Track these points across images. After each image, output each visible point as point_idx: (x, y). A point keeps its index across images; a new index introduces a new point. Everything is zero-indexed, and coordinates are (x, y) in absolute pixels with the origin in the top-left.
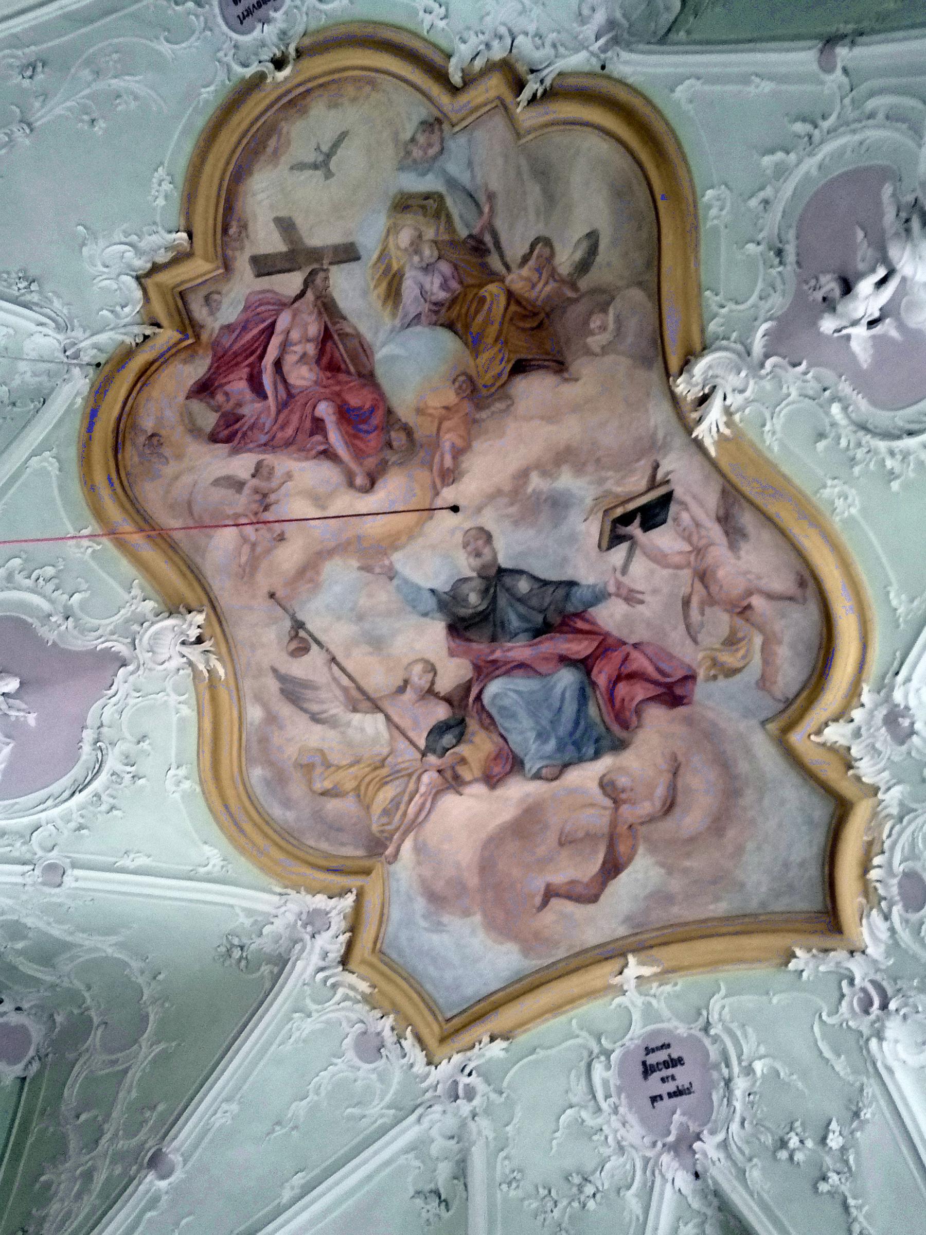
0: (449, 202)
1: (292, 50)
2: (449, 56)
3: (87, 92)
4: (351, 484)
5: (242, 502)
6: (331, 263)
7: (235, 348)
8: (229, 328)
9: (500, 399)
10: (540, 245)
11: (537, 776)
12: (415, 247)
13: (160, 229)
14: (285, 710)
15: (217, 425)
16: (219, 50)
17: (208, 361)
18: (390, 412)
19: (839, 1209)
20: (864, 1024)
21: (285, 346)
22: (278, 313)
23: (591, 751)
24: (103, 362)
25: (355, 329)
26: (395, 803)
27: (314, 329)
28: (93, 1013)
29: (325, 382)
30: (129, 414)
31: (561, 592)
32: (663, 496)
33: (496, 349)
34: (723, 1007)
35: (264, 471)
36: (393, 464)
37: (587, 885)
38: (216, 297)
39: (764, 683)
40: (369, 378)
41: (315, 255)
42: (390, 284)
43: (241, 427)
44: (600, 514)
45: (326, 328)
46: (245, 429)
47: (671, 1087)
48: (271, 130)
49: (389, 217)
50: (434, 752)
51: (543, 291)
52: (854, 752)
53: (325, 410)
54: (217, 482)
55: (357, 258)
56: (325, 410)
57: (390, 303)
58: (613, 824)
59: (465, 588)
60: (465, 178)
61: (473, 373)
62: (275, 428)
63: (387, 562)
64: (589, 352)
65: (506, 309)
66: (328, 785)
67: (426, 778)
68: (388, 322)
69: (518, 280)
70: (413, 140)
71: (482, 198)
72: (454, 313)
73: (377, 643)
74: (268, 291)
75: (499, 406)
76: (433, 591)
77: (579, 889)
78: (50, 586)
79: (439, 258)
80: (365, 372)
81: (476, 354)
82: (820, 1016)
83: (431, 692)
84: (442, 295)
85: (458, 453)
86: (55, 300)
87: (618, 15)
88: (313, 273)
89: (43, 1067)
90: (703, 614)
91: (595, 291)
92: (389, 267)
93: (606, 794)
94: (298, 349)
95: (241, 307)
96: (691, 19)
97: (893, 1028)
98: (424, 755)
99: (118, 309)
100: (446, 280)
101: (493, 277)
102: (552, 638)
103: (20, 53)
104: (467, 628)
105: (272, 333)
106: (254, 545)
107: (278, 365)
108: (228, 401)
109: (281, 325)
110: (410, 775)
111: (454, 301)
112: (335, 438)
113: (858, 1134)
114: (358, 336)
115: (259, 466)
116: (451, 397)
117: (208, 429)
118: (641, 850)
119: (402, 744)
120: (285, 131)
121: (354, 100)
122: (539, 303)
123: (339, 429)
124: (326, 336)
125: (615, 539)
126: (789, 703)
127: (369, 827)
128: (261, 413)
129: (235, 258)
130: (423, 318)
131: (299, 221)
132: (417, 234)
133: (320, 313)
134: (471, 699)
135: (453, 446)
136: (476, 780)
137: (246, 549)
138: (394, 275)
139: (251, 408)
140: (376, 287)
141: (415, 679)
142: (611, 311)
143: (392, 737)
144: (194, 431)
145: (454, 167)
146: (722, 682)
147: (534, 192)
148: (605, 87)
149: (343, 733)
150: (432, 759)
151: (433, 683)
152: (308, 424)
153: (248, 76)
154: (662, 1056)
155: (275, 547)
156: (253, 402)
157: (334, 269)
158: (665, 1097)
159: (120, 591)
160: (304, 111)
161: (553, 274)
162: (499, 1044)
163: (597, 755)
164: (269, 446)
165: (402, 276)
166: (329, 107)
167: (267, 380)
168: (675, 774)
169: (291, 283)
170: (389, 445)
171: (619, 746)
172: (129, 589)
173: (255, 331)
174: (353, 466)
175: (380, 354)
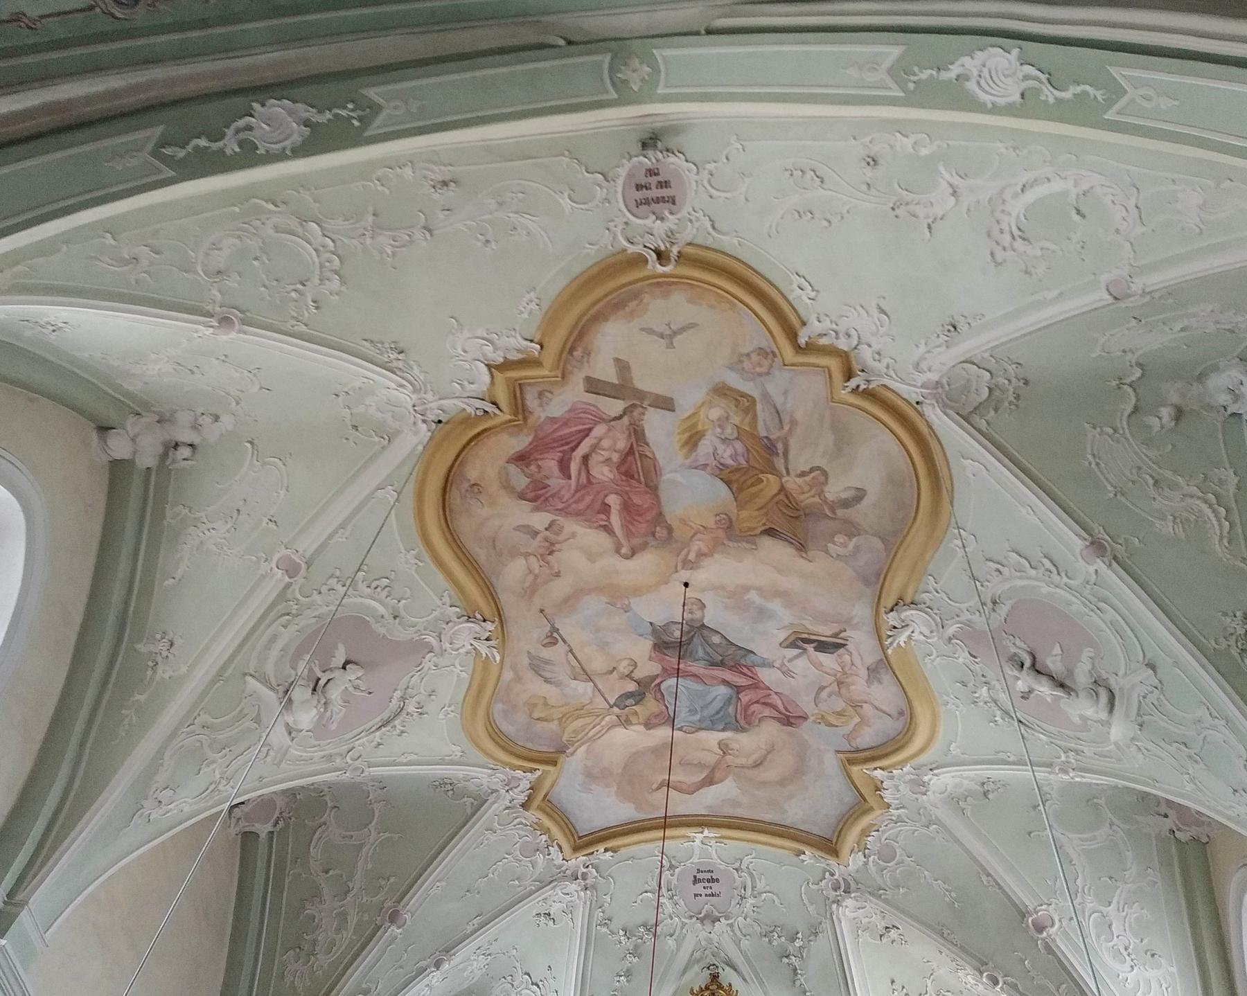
0: (759, 407)
1: (675, 250)
2: (804, 324)
3: (488, 217)
4: (618, 551)
5: (535, 544)
6: (649, 405)
7: (555, 435)
8: (553, 420)
9: (747, 542)
10: (819, 472)
12: (722, 422)
13: (518, 335)
14: (529, 675)
15: (527, 487)
16: (612, 221)
17: (530, 439)
18: (660, 514)
19: (791, 972)
21: (594, 448)
22: (596, 423)
23: (721, 727)
24: (443, 421)
25: (654, 454)
26: (583, 728)
27: (622, 444)
28: (327, 798)
29: (620, 483)
30: (459, 465)
31: (742, 652)
32: (841, 644)
33: (756, 513)
34: (751, 863)
35: (555, 528)
36: (652, 546)
37: (689, 785)
38: (547, 394)
39: (849, 737)
40: (653, 489)
41: (640, 395)
42: (690, 437)
43: (547, 492)
44: (791, 631)
45: (632, 445)
46: (547, 495)
47: (709, 891)
48: (636, 295)
49: (708, 394)
50: (618, 706)
51: (808, 499)
52: (884, 785)
53: (613, 500)
54: (517, 528)
55: (673, 410)
56: (613, 500)
57: (685, 450)
58: (718, 763)
59: (674, 627)
60: (779, 400)
61: (734, 519)
62: (571, 501)
63: (627, 602)
64: (827, 552)
65: (776, 495)
66: (542, 715)
67: (607, 719)
68: (680, 459)
69: (791, 483)
70: (748, 355)
71: (786, 419)
72: (735, 477)
73: (603, 646)
74: (594, 406)
75: (748, 546)
76: (651, 623)
77: (684, 787)
78: (385, 593)
79: (737, 439)
80: (651, 484)
81: (741, 505)
82: (808, 883)
83: (629, 676)
84: (729, 462)
85: (701, 555)
86: (415, 368)
87: (944, 381)
88: (634, 406)
89: (287, 826)
90: (829, 696)
91: (846, 521)
92: (695, 425)
93: (720, 748)
94: (606, 454)
95: (566, 408)
96: (992, 413)
97: (849, 902)
98: (611, 707)
99: (466, 383)
100: (736, 454)
101: (774, 471)
102: (723, 670)
103: (436, 169)
104: (666, 648)
105: (587, 435)
106: (536, 577)
107: (586, 459)
108: (539, 472)
109: (599, 430)
110: (598, 716)
111: (737, 470)
112: (615, 520)
113: (812, 943)
114: (654, 459)
116: (711, 523)
117: (519, 489)
118: (730, 778)
119: (599, 700)
120: (645, 301)
121: (712, 307)
122: (803, 504)
123: (620, 516)
124: (631, 451)
125: (793, 645)
126: (858, 751)
127: (561, 738)
128: (563, 487)
129: (572, 373)
130: (709, 468)
131: (633, 367)
132: (726, 415)
133: (630, 435)
134: (653, 685)
135: (699, 550)
136: (639, 724)
137: (531, 578)
138: (697, 432)
139: (556, 482)
140: (679, 434)
141: (621, 668)
142: (854, 540)
143: (594, 695)
144: (507, 486)
145: (771, 388)
146: (823, 727)
147: (828, 439)
149: (562, 690)
150: (616, 710)
151: (632, 672)
152: (597, 506)
153: (629, 251)
154: (708, 876)
155: (551, 580)
156: (558, 478)
157: (651, 410)
158: (703, 895)
159: (435, 598)
160: (666, 295)
161: (820, 494)
162: (609, 854)
163: (723, 730)
164: (565, 512)
165: (704, 435)
166: (689, 301)
167: (574, 467)
168: (769, 753)
169: (615, 407)
170: (654, 535)
171: (740, 729)
172: (441, 598)
173: (574, 429)
174: (623, 541)
175: (666, 477)
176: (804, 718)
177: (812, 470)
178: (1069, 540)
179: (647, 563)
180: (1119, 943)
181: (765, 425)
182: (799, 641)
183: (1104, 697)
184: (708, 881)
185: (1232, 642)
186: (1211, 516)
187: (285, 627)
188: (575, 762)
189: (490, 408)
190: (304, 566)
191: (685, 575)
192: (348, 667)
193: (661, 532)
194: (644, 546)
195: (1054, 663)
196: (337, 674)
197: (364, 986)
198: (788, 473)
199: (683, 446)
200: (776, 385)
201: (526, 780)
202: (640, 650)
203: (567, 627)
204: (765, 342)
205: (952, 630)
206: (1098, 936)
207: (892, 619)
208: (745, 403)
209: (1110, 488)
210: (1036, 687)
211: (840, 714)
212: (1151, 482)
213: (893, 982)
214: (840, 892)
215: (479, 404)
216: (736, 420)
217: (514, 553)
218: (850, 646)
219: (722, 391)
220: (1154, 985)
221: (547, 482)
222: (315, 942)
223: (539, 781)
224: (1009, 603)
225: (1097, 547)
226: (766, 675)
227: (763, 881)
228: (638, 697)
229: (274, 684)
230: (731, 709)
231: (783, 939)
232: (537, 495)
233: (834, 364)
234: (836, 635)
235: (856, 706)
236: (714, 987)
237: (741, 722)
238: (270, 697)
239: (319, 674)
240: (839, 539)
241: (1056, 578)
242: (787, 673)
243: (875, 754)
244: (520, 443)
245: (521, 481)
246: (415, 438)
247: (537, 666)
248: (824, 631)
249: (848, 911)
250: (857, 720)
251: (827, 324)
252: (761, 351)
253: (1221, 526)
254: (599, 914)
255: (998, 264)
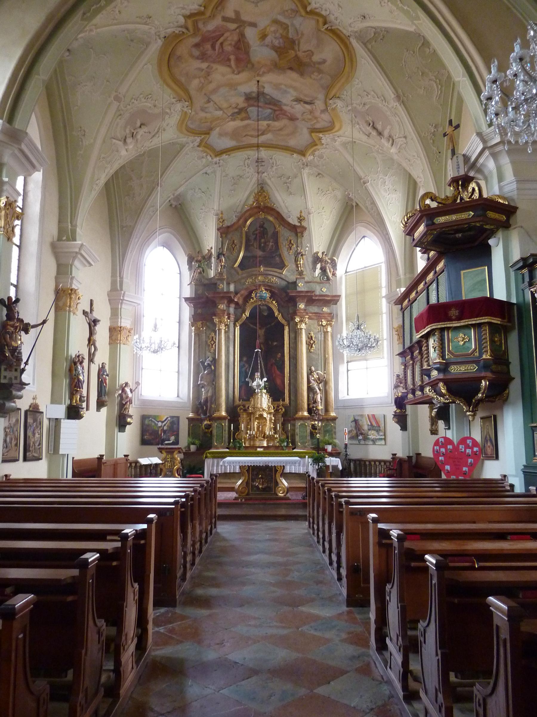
0: (290, 28)
4: (233, 72)
8: (209, 31)
11: (253, 120)
12: (275, 32)
17: (200, 38)
20: (302, 166)
21: (225, 40)
27: (236, 38)
40: (247, 53)
41: (244, 22)
51: (306, 60)
53: (232, 57)
60: (298, 26)
64: (311, 77)
69: (300, 54)
70: (287, 11)
78: (151, 100)
83: (236, 108)
85: (264, 73)
94: (229, 42)
96: (374, 42)
107: (222, 44)
109: (226, 35)
112: (233, 63)
115: (209, 66)
124: (239, 40)
126: (314, 129)
137: (201, 84)
139: (210, 52)
144: (192, 56)
148: (346, 40)
150: (231, 117)
161: (310, 59)
164: (214, 62)
167: (217, 46)
169: (233, 26)
171: (274, 120)
176: (298, 119)
177: (308, 51)
178: (390, 93)
179: (244, 76)
180: (387, 187)
181: (291, 34)
182: (298, 100)
183: (391, 142)
184: (261, 162)
185: (429, 134)
186: (436, 88)
187: (120, 119)
188: (215, 133)
189: (184, 30)
190: (123, 98)
191: (258, 78)
192: (142, 127)
193: (249, 66)
194: (243, 71)
195: (379, 127)
196: (139, 130)
197: (152, 205)
198: (299, 51)
199: (259, 39)
200: (298, 21)
201: (198, 140)
202: (241, 101)
203: (214, 97)
204: (294, 7)
205: (350, 108)
206: (381, 185)
207: (331, 102)
208: (285, 27)
209: (407, 75)
210: (372, 133)
211: (310, 119)
212: (421, 74)
213: (319, 189)
214: (305, 166)
215: (180, 29)
216: (281, 31)
217: (195, 77)
218: (316, 104)
219: (276, 22)
220: (394, 199)
221: (207, 52)
222: (134, 194)
223: (203, 138)
224: (369, 106)
225: (398, 97)
226: (285, 108)
227: (279, 162)
228: (239, 113)
229: (120, 139)
230: (272, 115)
231: (285, 179)
232: (203, 57)
233: (321, 20)
234: (311, 101)
235: (316, 118)
236: (262, 191)
237: (276, 118)
238: (121, 143)
239: (133, 131)
240: (316, 74)
241: (384, 103)
242: (293, 108)
243: (320, 131)
244: (197, 40)
245: (196, 52)
246: (156, 45)
247: (203, 109)
248: (307, 99)
249: (306, 172)
250: (315, 121)
251: (318, 5)
252: (292, 10)
253: (438, 91)
254: (224, 174)
255: (381, 6)
